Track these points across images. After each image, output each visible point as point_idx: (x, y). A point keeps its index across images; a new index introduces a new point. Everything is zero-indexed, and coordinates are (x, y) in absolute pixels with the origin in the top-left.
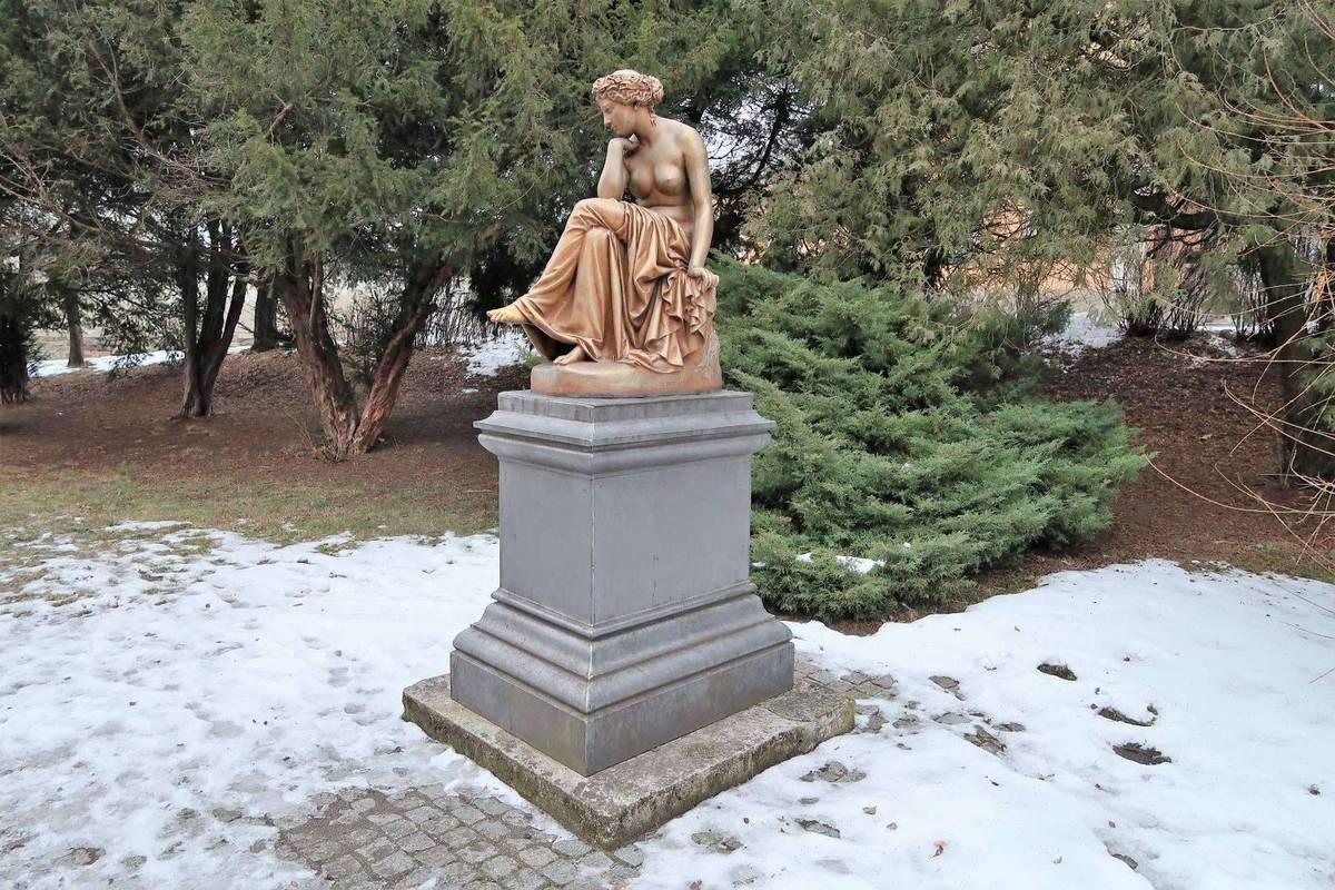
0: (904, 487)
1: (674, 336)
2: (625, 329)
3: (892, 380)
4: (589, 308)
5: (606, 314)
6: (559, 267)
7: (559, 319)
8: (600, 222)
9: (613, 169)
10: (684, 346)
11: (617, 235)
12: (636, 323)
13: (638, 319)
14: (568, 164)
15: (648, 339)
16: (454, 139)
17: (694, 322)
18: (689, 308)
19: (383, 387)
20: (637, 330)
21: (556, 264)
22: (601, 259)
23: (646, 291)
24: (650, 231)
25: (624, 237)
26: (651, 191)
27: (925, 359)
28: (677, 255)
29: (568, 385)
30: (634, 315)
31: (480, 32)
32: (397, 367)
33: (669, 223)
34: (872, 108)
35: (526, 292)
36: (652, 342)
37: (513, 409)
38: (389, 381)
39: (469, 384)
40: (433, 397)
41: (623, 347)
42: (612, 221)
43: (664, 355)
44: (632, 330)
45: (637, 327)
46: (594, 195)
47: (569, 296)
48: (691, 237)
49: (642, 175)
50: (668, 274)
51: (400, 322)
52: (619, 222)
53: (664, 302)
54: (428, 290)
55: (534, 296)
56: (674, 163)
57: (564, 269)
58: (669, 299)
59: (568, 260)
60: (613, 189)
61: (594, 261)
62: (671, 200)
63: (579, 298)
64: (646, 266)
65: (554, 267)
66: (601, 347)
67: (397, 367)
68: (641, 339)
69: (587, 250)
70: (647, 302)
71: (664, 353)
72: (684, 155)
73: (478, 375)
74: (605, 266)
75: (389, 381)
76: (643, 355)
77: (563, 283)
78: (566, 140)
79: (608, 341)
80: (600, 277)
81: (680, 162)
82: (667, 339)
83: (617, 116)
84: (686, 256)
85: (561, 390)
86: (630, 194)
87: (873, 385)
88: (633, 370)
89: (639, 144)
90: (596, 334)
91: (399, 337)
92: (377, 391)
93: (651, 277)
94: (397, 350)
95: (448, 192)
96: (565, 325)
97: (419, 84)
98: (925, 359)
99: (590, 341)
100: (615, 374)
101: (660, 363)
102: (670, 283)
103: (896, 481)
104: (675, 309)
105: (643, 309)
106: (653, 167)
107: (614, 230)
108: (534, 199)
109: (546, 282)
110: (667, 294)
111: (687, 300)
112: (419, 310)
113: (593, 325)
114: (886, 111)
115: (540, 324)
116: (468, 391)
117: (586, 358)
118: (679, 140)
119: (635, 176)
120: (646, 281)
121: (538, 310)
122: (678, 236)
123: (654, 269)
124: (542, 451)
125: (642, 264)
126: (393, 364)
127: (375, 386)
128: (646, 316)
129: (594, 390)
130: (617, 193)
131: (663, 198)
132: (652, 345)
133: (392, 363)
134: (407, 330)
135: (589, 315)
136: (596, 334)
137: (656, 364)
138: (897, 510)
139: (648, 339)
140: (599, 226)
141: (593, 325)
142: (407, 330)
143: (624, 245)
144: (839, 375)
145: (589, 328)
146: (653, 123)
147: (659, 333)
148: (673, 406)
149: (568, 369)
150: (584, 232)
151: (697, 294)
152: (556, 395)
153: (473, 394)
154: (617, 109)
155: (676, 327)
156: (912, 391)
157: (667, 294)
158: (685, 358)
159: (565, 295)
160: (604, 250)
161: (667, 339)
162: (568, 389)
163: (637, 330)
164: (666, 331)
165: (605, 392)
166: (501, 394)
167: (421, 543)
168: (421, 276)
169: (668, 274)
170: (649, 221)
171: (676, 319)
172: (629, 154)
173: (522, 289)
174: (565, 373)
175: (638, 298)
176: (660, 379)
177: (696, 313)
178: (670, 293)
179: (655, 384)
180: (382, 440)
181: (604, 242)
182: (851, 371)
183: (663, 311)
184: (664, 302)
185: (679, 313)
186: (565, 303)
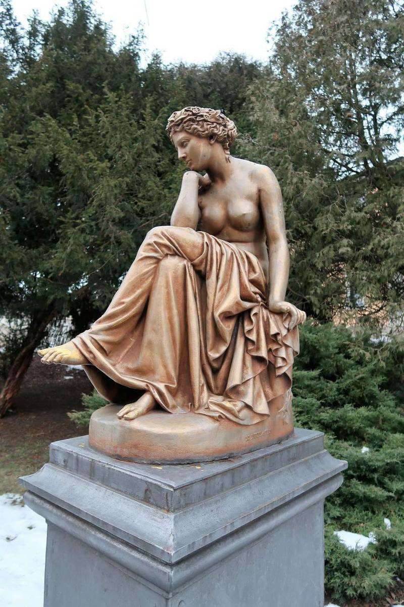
0: (375, 470)
1: (257, 378)
2: (200, 376)
3: (343, 386)
4: (161, 348)
5: (181, 354)
6: (128, 300)
7: (127, 358)
8: (176, 250)
9: (187, 196)
10: (268, 390)
11: (194, 266)
12: (215, 365)
13: (217, 360)
14: (130, 250)
15: (231, 384)
16: (60, 231)
17: (280, 363)
18: (274, 347)
19: (14, 379)
20: (215, 372)
21: (124, 296)
22: (176, 292)
23: (227, 328)
24: (230, 262)
25: (202, 268)
26: (223, 227)
27: (362, 372)
28: (257, 290)
29: (136, 446)
30: (213, 355)
31: (80, 169)
32: (22, 367)
33: (248, 257)
34: (311, 219)
35: (88, 328)
36: (235, 388)
37: (65, 467)
38: (17, 376)
39: (68, 374)
40: (48, 382)
41: (201, 392)
42: (189, 250)
43: (250, 403)
44: (209, 372)
45: (216, 370)
46: (169, 224)
47: (137, 333)
48: (267, 272)
49: (216, 212)
50: (250, 310)
51: (26, 340)
52: (197, 251)
53: (247, 340)
54: (43, 324)
55: (96, 333)
56: (249, 198)
57: (134, 303)
58: (253, 337)
59: (139, 292)
60: (189, 219)
61: (168, 294)
62: (244, 236)
63: (149, 335)
64: (230, 300)
65: (123, 298)
66: (173, 393)
67: (22, 367)
68: (220, 383)
69: (161, 282)
70: (228, 338)
71: (249, 400)
72: (260, 191)
73: (73, 369)
74: (181, 301)
75: (17, 376)
76: (227, 404)
77: (134, 316)
78: (130, 235)
79: (183, 383)
80: (175, 311)
81: (255, 197)
82: (251, 382)
83: (192, 148)
84: (265, 290)
85: (126, 452)
86: (202, 224)
87: (331, 390)
88: (217, 424)
89: (213, 176)
90: (168, 376)
91: (24, 351)
92: (10, 381)
93: (235, 313)
94: (23, 358)
95: (53, 262)
96: (131, 366)
97: (40, 199)
98: (362, 372)
99: (162, 387)
100: (191, 429)
101: (245, 412)
102: (253, 318)
103: (369, 466)
104: (258, 349)
105: (223, 349)
106: (226, 203)
107: (191, 260)
108: (108, 271)
109: (111, 317)
110: (250, 331)
111: (273, 339)
112: (37, 335)
113: (165, 367)
114: (319, 221)
115: (102, 366)
116: (67, 378)
117: (157, 407)
118: (253, 176)
119: (207, 212)
120: (227, 316)
121: (101, 349)
122: (257, 269)
123: (237, 303)
124: (96, 539)
125: (224, 296)
126: (20, 367)
127: (8, 379)
128: (227, 357)
129: (169, 454)
130: (191, 224)
131: (236, 234)
132: (236, 391)
133: (19, 366)
134: (29, 346)
135: (162, 357)
136: (168, 376)
137: (241, 415)
138: (375, 491)
139: (231, 384)
140: (175, 254)
141: (165, 367)
142: (29, 346)
143: (202, 277)
144: (307, 382)
145: (161, 370)
146: (228, 160)
147: (243, 377)
148: (260, 465)
149: (136, 425)
150: (158, 261)
151: (284, 332)
152: (119, 458)
153: (70, 380)
154: (194, 141)
155: (260, 369)
156: (357, 392)
157: (250, 331)
158: (270, 403)
159: (132, 332)
160: (180, 280)
161: (251, 382)
162: (135, 451)
163: (215, 372)
164: (250, 374)
165: (183, 457)
166: (56, 444)
167: (14, 503)
168: (39, 316)
169: (250, 310)
170: (230, 252)
171: (260, 360)
172: (204, 190)
173: (81, 326)
174: (131, 431)
175: (218, 336)
176: (246, 433)
177: (283, 353)
178: (254, 330)
179: (243, 438)
180: (11, 411)
181: (180, 272)
182: (312, 379)
183: (246, 350)
184: (247, 340)
185: (263, 353)
186: (133, 340)
